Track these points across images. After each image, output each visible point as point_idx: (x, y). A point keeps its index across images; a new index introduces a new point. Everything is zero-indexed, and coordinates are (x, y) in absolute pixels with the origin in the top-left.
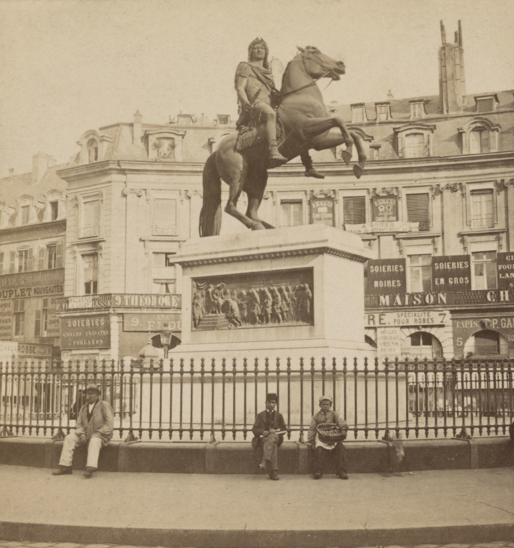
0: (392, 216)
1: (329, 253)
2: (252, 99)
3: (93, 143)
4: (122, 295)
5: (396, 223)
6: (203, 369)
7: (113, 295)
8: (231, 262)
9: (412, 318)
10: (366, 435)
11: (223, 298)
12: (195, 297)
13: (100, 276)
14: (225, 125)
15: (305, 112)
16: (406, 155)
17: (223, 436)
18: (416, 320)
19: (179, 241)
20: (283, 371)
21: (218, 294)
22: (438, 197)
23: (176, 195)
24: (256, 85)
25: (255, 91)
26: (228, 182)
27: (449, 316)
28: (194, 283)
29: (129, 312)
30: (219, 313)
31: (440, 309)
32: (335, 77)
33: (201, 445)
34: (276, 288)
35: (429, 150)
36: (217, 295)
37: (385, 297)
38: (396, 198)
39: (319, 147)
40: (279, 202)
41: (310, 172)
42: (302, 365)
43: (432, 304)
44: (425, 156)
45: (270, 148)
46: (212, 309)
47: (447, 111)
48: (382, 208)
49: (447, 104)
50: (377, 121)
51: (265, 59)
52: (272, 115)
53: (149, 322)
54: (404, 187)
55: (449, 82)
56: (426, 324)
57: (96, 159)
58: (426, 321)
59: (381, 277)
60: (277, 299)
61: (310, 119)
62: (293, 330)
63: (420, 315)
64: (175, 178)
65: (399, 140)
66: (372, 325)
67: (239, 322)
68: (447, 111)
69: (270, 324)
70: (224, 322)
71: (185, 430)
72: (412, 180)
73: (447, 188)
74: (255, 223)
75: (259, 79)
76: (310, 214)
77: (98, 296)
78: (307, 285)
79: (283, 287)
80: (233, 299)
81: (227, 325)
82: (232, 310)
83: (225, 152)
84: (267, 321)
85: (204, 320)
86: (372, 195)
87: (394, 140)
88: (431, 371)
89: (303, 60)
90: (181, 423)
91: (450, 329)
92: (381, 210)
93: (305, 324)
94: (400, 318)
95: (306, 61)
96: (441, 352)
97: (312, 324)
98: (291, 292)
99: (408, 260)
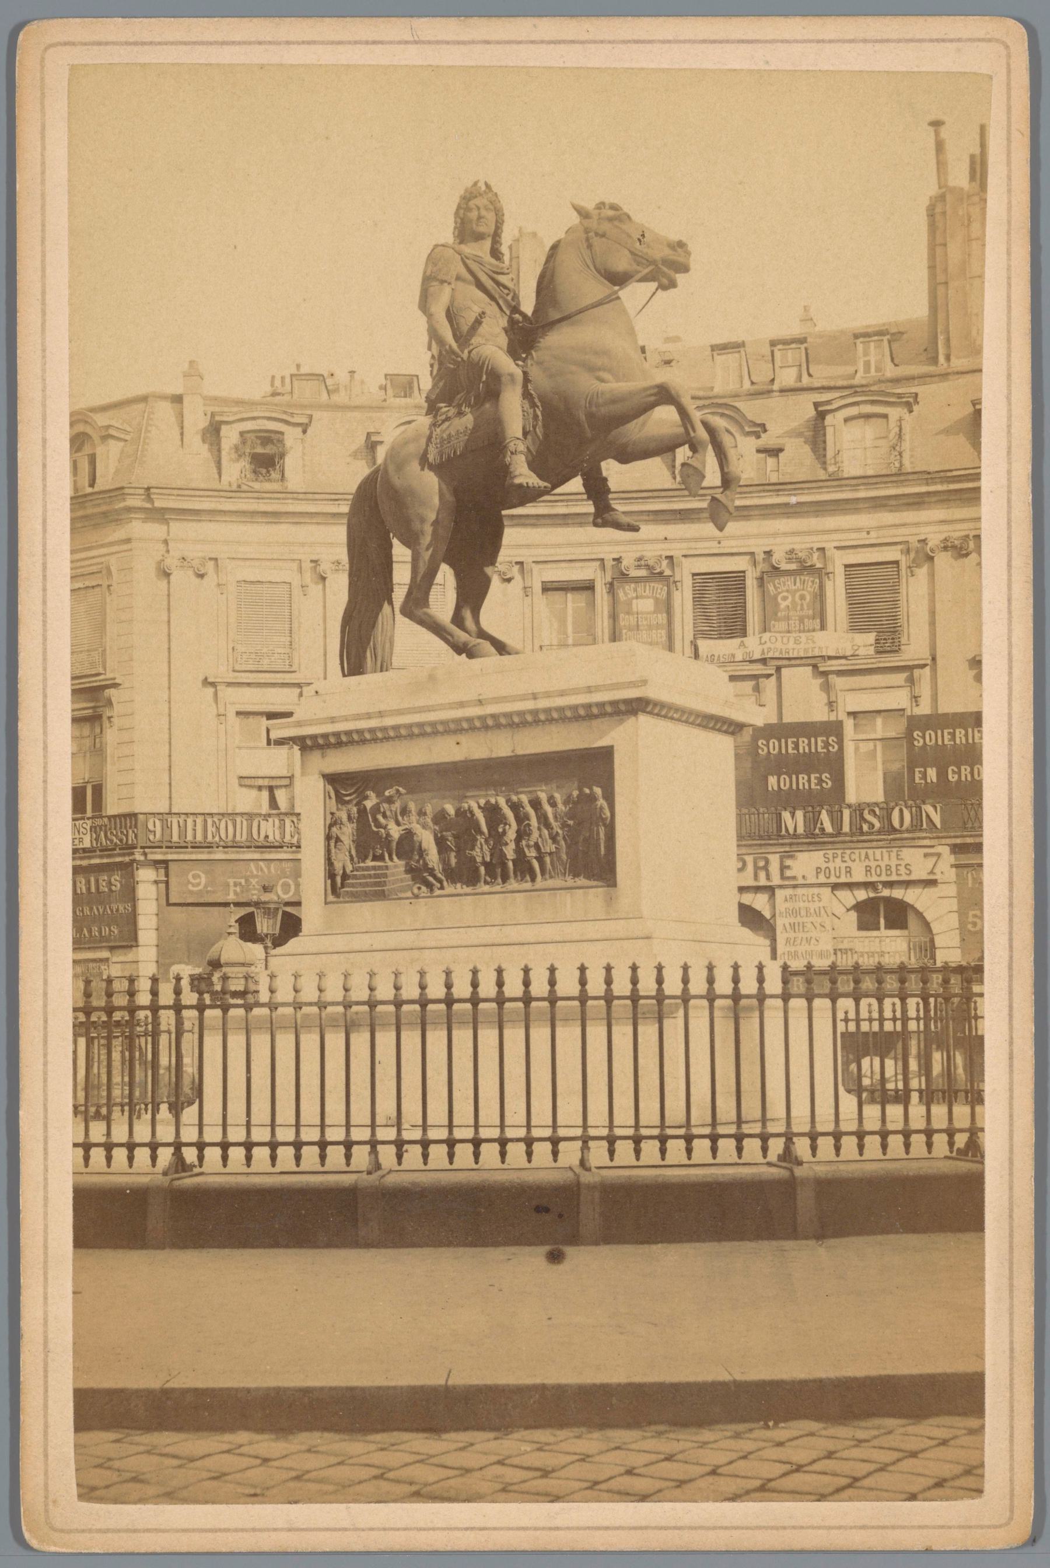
0: (808, 617)
1: (650, 713)
2: (463, 338)
3: (82, 444)
4: (164, 817)
5: (819, 635)
6: (475, 993)
7: (141, 817)
8: (346, 744)
9: (859, 865)
10: (740, 1150)
11: (398, 824)
12: (334, 823)
13: (110, 768)
14: (408, 400)
15: (591, 369)
16: (846, 470)
17: (399, 1157)
18: (868, 869)
19: (299, 685)
20: (460, 1001)
21: (388, 813)
22: (923, 572)
23: (288, 574)
24: (474, 302)
25: (470, 317)
26: (406, 543)
27: (948, 858)
28: (330, 788)
29: (182, 857)
30: (391, 859)
31: (926, 842)
32: (665, 281)
33: (347, 1180)
34: (524, 799)
35: (900, 454)
36: (385, 816)
37: (793, 815)
38: (821, 574)
39: (625, 456)
40: (537, 587)
41: (603, 515)
42: (583, 982)
43: (908, 831)
44: (894, 471)
45: (508, 459)
46: (374, 849)
47: (948, 358)
48: (785, 598)
49: (948, 340)
50: (776, 387)
51: (496, 237)
52: (511, 375)
53: (231, 881)
54: (837, 548)
55: (951, 285)
56: (894, 878)
57: (92, 484)
58: (894, 869)
59: (782, 765)
60: (529, 825)
61: (602, 387)
62: (566, 897)
63: (878, 857)
64: (284, 531)
65: (829, 431)
66: (763, 881)
67: (440, 881)
68: (948, 358)
69: (513, 884)
70: (402, 880)
71: (383, 1143)
72: (858, 530)
73: (945, 548)
74: (474, 641)
75: (480, 286)
76: (614, 617)
77: (106, 820)
78: (598, 791)
79: (543, 796)
80: (424, 826)
81: (411, 888)
82: (422, 852)
83: (400, 468)
84: (505, 879)
85: (355, 877)
86: (762, 567)
87: (816, 433)
88: (799, 996)
89: (587, 239)
90: (450, 1126)
91: (952, 890)
92: (783, 604)
93: (595, 883)
94: (831, 865)
95: (596, 241)
96: (930, 948)
97: (614, 885)
98: (561, 807)
99: (849, 725)
